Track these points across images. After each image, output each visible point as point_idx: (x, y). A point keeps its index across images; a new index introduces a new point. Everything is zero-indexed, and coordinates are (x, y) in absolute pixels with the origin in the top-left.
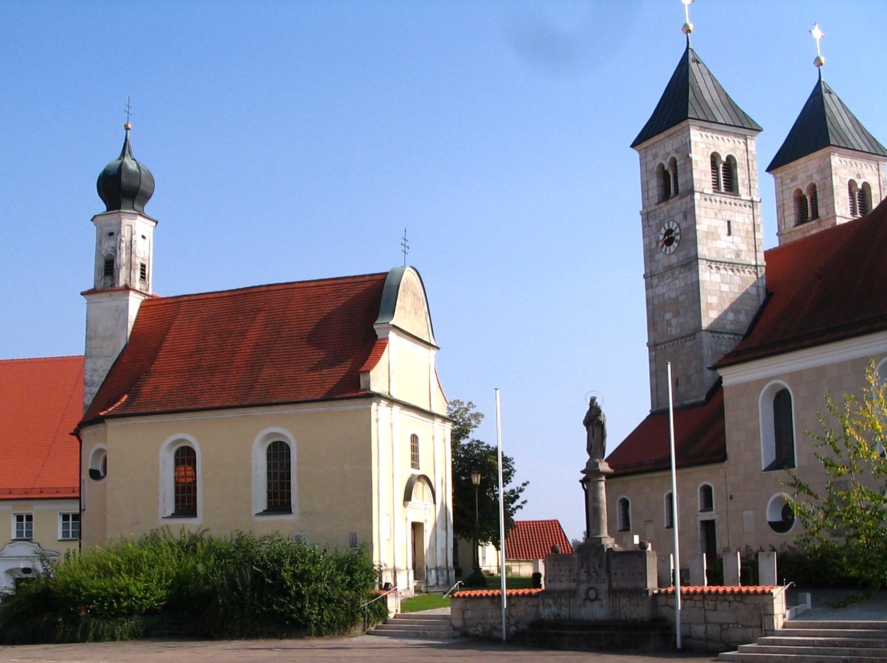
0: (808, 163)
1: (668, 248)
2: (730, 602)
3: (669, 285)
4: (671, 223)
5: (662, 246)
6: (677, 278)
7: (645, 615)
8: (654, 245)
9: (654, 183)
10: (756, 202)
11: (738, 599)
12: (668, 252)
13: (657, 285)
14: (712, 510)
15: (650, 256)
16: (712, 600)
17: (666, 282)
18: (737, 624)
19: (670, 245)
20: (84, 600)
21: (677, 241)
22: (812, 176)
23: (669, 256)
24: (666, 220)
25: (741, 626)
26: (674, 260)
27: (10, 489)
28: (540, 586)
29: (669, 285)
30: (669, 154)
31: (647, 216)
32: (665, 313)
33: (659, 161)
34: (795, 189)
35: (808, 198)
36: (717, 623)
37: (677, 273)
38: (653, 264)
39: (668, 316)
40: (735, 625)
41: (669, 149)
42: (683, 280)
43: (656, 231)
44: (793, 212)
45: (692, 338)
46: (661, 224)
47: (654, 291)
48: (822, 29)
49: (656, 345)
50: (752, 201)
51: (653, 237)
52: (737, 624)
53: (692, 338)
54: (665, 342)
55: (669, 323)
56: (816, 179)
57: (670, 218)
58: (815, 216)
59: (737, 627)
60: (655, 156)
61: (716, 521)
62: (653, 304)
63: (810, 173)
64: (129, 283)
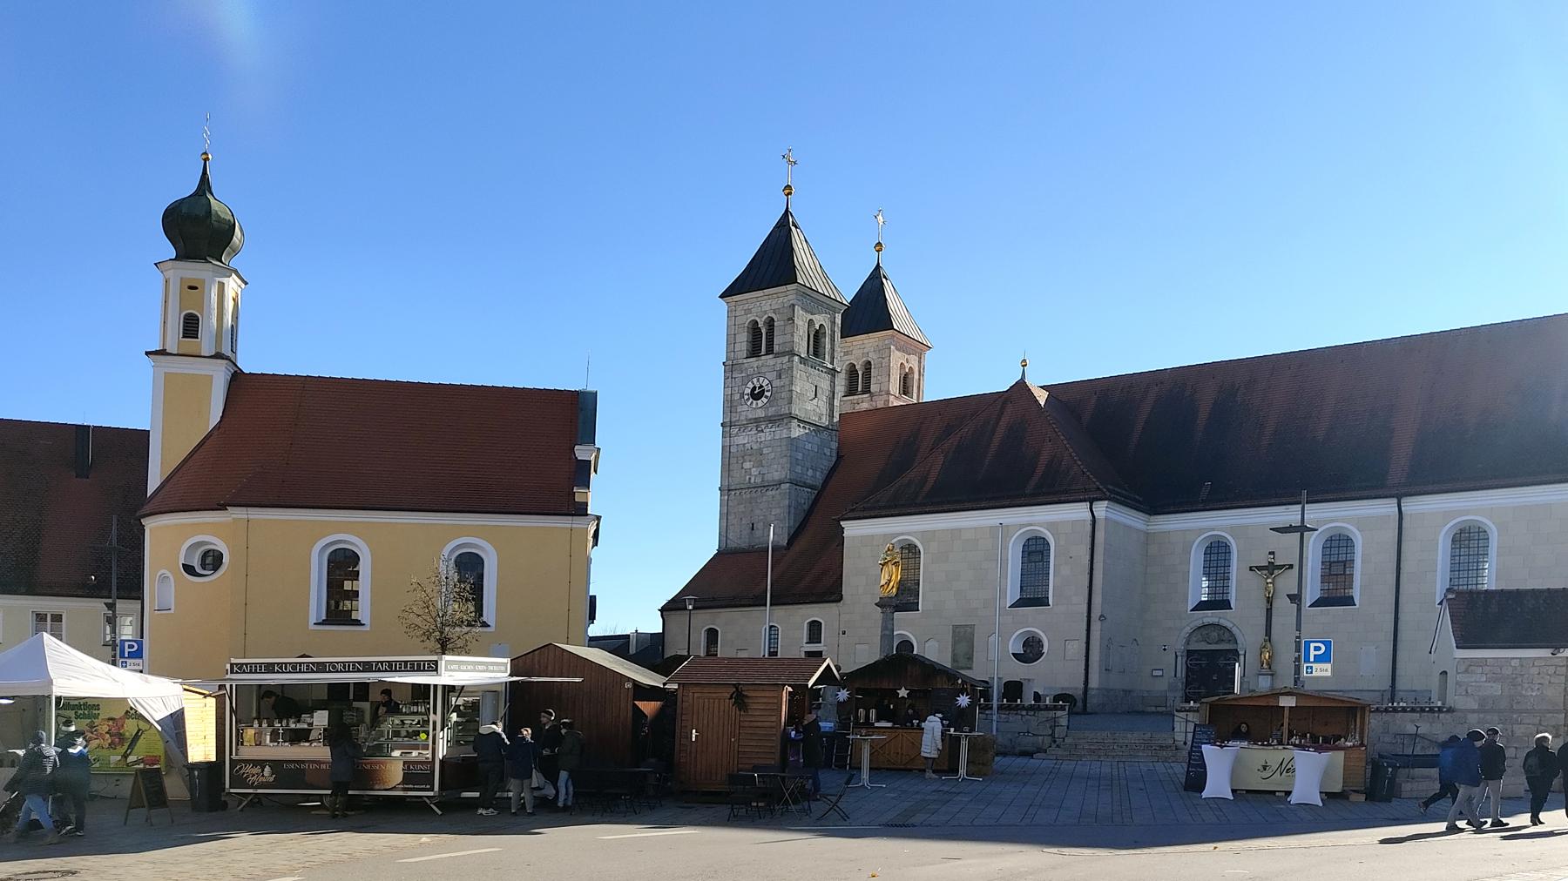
0: (866, 341)
1: (755, 402)
4: (761, 379)
5: (748, 399)
6: (762, 431)
8: (737, 397)
9: (743, 338)
10: (838, 372)
12: (754, 406)
13: (737, 435)
14: (820, 642)
15: (730, 405)
17: (748, 433)
18: (1028, 732)
19: (755, 400)
20: (477, 809)
21: (766, 397)
22: (868, 353)
23: (758, 408)
26: (760, 413)
28: (878, 720)
30: (765, 312)
31: (731, 367)
33: (751, 317)
34: (848, 362)
36: (128, 811)
37: (763, 427)
38: (733, 414)
39: (747, 465)
41: (767, 308)
44: (843, 383)
45: (775, 488)
46: (749, 378)
49: (729, 490)
50: (834, 369)
51: (736, 389)
52: (1028, 732)
53: (775, 488)
54: (745, 489)
55: (748, 471)
56: (872, 357)
57: (760, 374)
58: (867, 390)
60: (748, 311)
61: (823, 653)
62: (730, 452)
63: (866, 351)
64: (236, 369)
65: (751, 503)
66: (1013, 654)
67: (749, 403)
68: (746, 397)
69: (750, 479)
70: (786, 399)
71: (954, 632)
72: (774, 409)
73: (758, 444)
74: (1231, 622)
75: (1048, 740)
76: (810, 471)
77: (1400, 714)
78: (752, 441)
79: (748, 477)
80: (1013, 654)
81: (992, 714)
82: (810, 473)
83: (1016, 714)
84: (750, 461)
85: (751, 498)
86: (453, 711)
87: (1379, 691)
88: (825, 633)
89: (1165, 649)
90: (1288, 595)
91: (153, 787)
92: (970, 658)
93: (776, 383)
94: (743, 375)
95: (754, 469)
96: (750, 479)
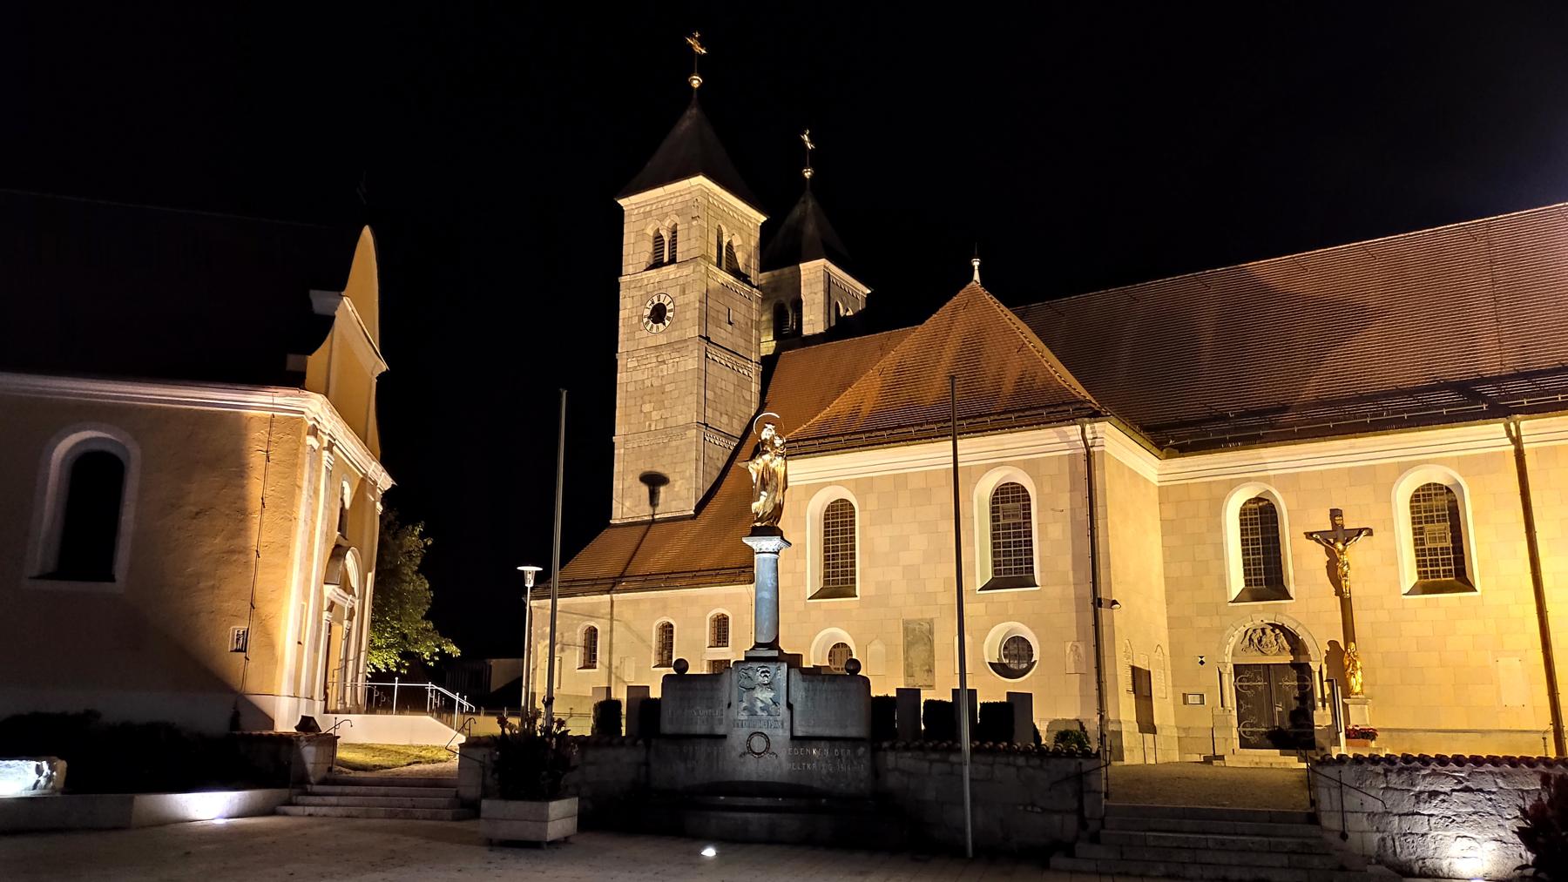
1: (655, 325)
2: (1019, 768)
3: (652, 371)
4: (662, 296)
6: (664, 362)
7: (862, 785)
11: (1037, 762)
12: (654, 331)
16: (984, 764)
18: (1033, 805)
24: (656, 293)
25: (1039, 810)
26: (662, 340)
27: (930, 504)
29: (652, 371)
32: (644, 403)
35: (666, 239)
39: (647, 408)
40: (1029, 808)
42: (673, 366)
43: (639, 304)
47: (1513, 427)
48: (700, 56)
59: (1032, 812)
65: (651, 458)
66: (990, 663)
67: (648, 328)
68: (645, 320)
69: (650, 425)
70: (691, 320)
71: (906, 629)
72: (677, 333)
73: (660, 380)
74: (1295, 621)
75: (1072, 822)
76: (725, 417)
77: (1064, 760)
78: (652, 376)
79: (647, 423)
80: (990, 663)
81: (960, 764)
82: (725, 419)
83: (1008, 764)
84: (650, 402)
85: (651, 450)
86: (1098, 752)
87: (1538, 732)
88: (733, 635)
89: (1202, 663)
90: (1133, 668)
91: (322, 825)
92: (930, 671)
93: (680, 300)
94: (642, 293)
95: (655, 412)
96: (650, 425)
